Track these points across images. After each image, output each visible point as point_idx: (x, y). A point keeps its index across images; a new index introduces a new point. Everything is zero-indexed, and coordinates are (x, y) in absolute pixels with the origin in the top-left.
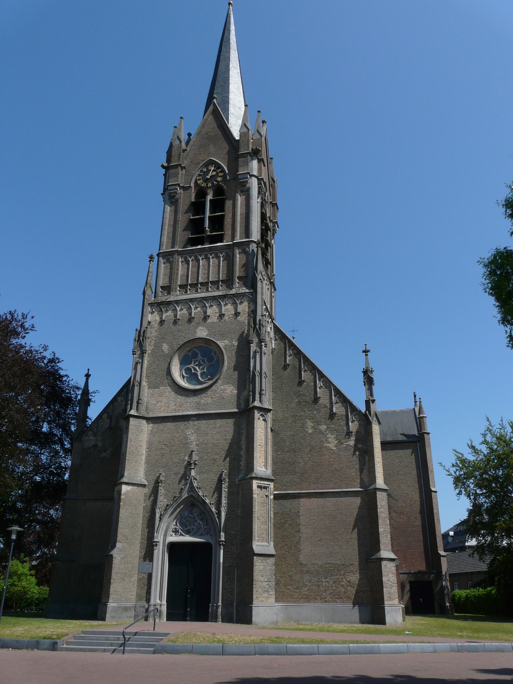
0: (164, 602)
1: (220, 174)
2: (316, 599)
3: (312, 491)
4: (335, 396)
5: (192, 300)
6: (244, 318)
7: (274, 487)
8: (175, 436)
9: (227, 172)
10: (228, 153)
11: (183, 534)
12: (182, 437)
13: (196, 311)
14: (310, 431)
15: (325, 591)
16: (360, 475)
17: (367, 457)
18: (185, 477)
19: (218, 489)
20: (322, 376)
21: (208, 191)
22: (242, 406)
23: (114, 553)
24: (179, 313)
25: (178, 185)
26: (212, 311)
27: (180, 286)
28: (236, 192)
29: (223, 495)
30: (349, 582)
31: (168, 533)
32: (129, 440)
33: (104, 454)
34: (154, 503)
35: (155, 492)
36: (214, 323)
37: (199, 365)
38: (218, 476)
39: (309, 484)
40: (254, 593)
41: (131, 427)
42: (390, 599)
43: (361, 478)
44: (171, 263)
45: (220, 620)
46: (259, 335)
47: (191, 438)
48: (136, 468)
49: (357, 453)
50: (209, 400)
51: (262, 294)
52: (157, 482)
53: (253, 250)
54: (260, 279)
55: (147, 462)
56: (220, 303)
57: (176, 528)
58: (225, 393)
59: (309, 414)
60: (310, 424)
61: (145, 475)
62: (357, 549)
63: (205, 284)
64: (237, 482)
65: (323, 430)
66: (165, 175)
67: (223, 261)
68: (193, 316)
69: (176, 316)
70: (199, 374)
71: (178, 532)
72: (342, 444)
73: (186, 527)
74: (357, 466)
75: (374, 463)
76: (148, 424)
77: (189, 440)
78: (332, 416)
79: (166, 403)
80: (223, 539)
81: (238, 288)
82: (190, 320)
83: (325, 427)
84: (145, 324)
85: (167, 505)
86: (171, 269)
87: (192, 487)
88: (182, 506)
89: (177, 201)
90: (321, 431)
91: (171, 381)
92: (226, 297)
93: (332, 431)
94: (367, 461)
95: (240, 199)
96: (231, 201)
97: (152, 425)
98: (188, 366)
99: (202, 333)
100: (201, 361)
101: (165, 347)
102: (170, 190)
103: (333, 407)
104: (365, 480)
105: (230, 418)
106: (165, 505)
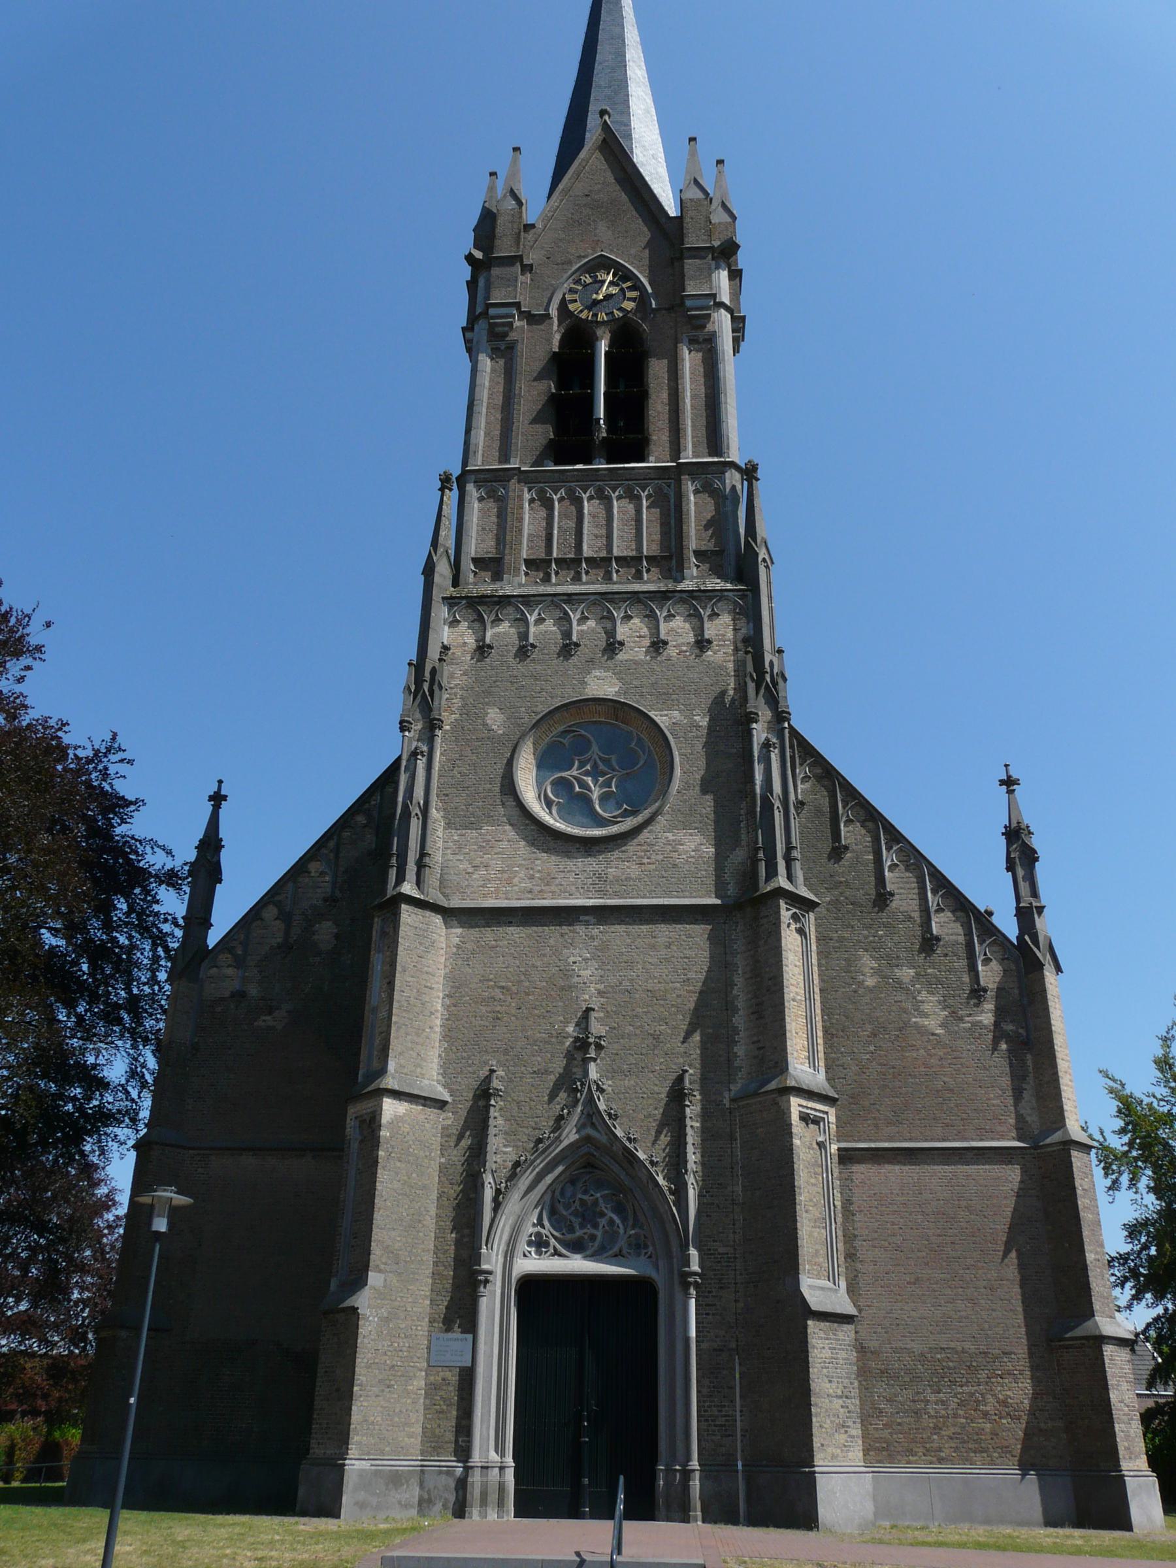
0: (509, 1460)
1: (629, 294)
2: (911, 1452)
3: (886, 1145)
4: (934, 892)
5: (570, 598)
6: (722, 655)
7: (837, 1117)
8: (533, 966)
9: (650, 290)
10: (649, 245)
11: (564, 1251)
12: (554, 970)
13: (585, 628)
14: (870, 982)
15: (937, 1429)
16: (1016, 1105)
17: (1029, 1057)
18: (570, 1082)
19: (673, 1119)
20: (895, 836)
21: (599, 332)
22: (732, 890)
23: (363, 1301)
24: (532, 629)
25: (517, 305)
26: (632, 630)
27: (529, 563)
28: (677, 341)
29: (690, 1140)
30: (1004, 1403)
31: (520, 1250)
32: (399, 968)
33: (266, 1020)
34: (477, 1154)
35: (476, 1124)
36: (636, 663)
37: (595, 773)
38: (669, 1083)
39: (876, 1126)
40: (815, 1430)
41: (403, 930)
42: (1132, 1456)
43: (1017, 1112)
44: (502, 502)
45: (699, 1513)
46: (773, 701)
47: (582, 973)
48: (419, 1054)
49: (1004, 1046)
50: (634, 870)
51: (770, 597)
52: (484, 1094)
53: (734, 487)
54: (764, 560)
55: (448, 1035)
56: (652, 611)
57: (538, 1234)
58: (678, 853)
59: (866, 937)
60: (868, 962)
61: (444, 1074)
62: (1020, 1309)
63: (601, 563)
64: (726, 1102)
65: (906, 980)
66: (472, 285)
67: (648, 507)
68: (574, 639)
69: (524, 636)
70: (595, 796)
71: (547, 1244)
72: (961, 1019)
73: (571, 1230)
74: (1006, 1082)
75: (1056, 1073)
76: (447, 925)
77: (576, 979)
78: (929, 943)
79: (503, 872)
80: (695, 1267)
81: (694, 578)
82: (568, 649)
83: (912, 972)
84: (433, 652)
85: (517, 1164)
86: (502, 515)
87: (592, 1115)
88: (560, 1168)
89: (511, 347)
90: (900, 983)
91: (516, 812)
92: (669, 599)
93: (931, 985)
94: (1031, 1069)
95: (689, 360)
96: (665, 361)
97: (459, 931)
98: (563, 774)
99: (603, 685)
100: (599, 762)
101: (495, 718)
102: (493, 318)
103: (929, 919)
104: (1028, 1119)
105: (695, 922)
106: (510, 1164)
